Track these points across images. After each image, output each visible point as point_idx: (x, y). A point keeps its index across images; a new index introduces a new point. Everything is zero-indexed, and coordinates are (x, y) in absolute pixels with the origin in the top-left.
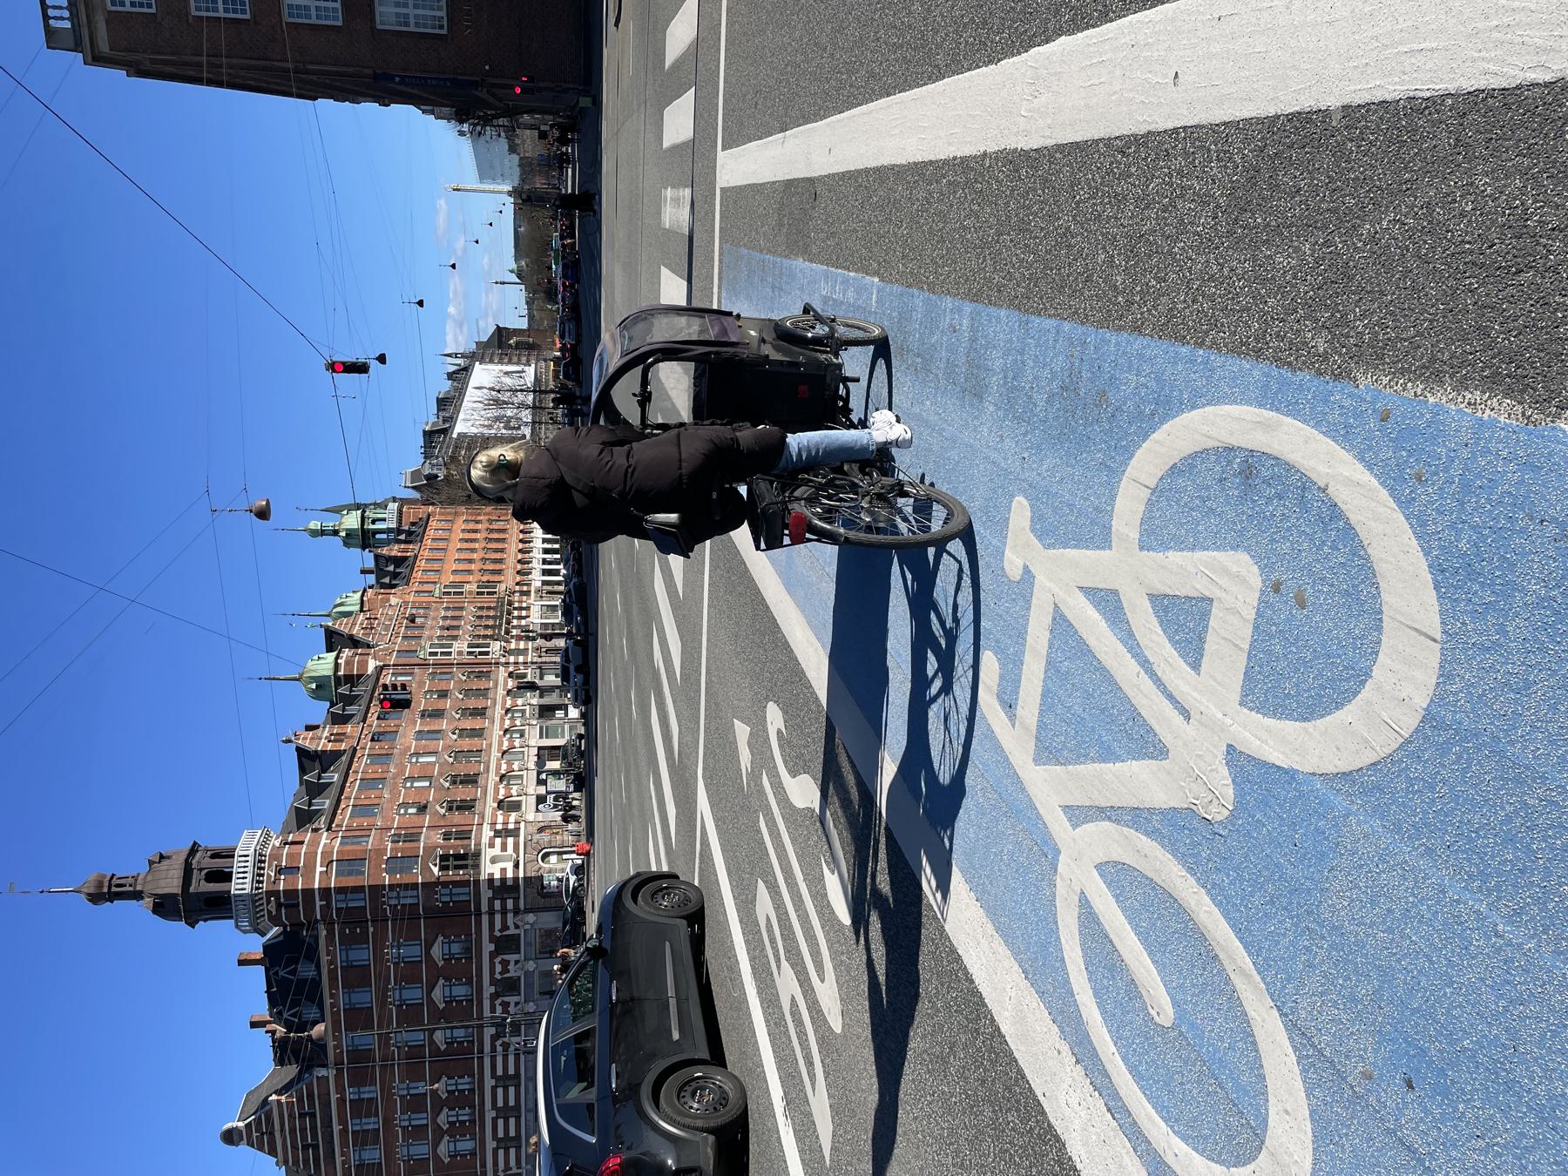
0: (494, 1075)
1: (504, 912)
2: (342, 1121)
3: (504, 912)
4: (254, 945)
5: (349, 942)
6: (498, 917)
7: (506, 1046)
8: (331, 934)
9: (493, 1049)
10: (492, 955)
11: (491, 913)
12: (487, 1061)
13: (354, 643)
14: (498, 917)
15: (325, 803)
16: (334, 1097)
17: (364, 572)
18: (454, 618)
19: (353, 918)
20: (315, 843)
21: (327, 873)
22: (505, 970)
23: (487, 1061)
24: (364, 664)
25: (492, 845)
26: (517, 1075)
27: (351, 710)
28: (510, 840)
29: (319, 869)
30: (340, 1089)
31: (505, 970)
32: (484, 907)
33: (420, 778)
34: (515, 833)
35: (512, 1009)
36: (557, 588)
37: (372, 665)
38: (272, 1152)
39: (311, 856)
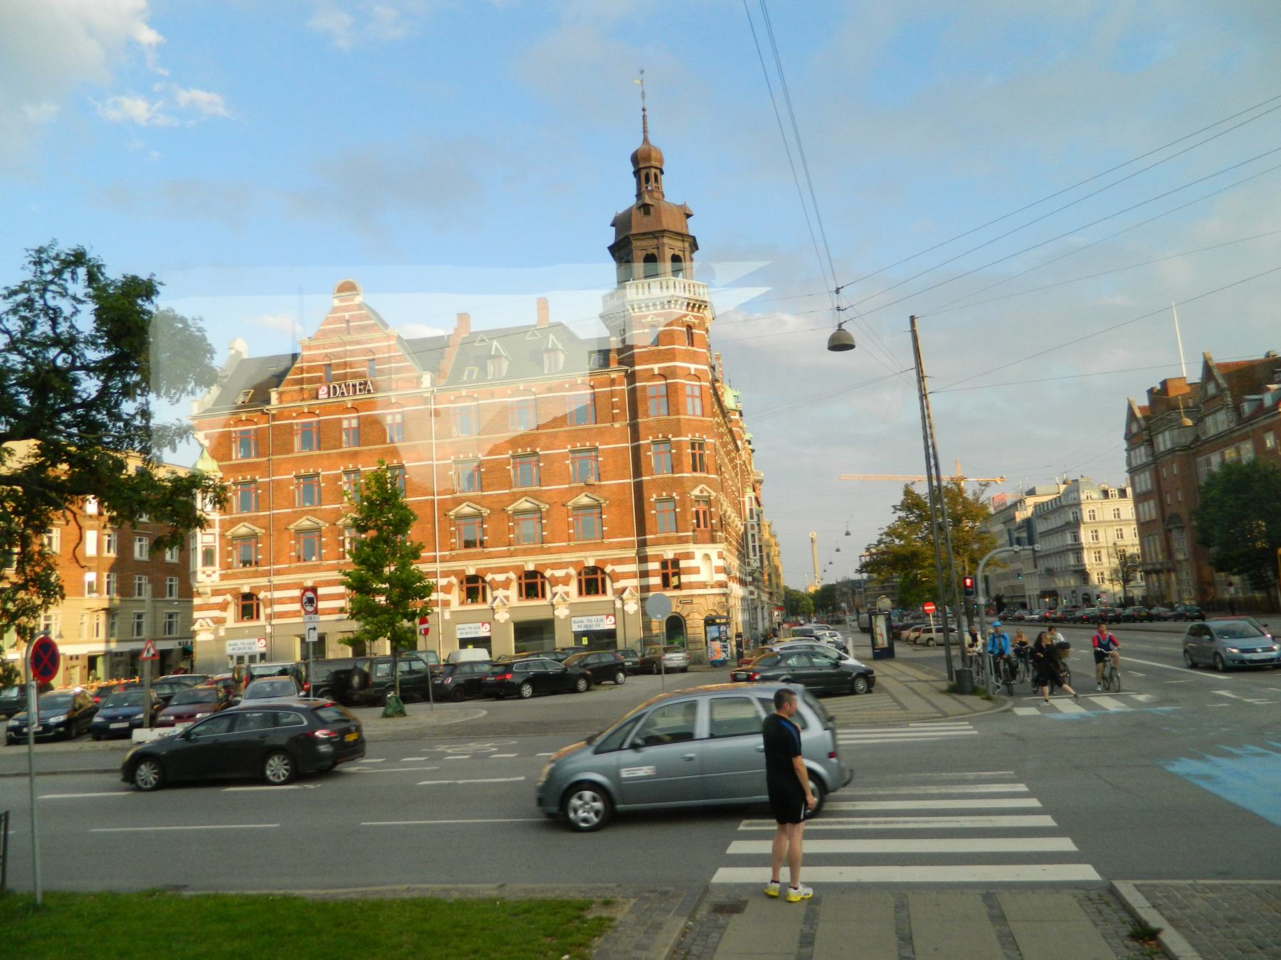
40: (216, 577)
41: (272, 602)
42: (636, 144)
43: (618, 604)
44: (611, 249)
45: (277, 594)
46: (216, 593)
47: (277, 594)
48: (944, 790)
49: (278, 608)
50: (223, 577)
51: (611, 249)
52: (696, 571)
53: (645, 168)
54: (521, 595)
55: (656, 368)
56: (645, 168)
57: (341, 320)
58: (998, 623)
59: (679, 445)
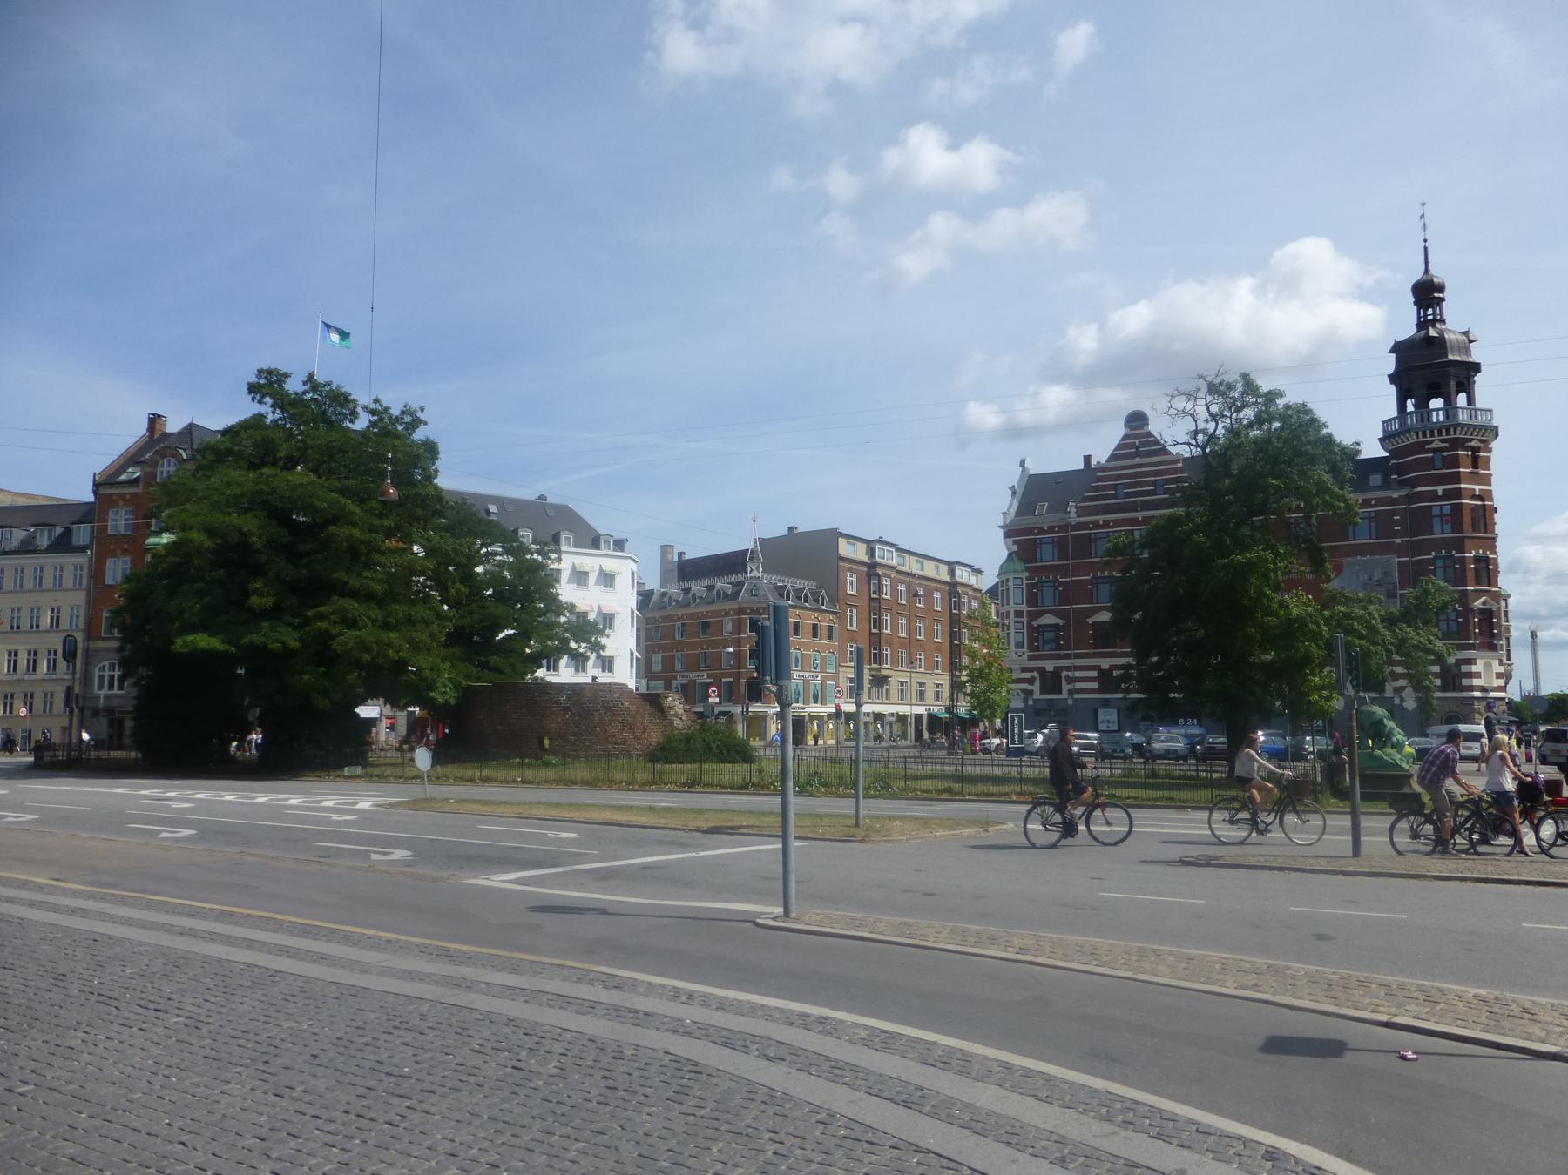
5: (1382, 524)
7: (1031, 681)
29: (1477, 488)
38: (1113, 457)
40: (1025, 657)
41: (1070, 680)
42: (1418, 275)
43: (1397, 701)
44: (1390, 377)
45: (1078, 674)
46: (1024, 670)
47: (1078, 674)
48: (237, 931)
49: (1079, 685)
50: (1031, 658)
51: (1390, 377)
52: (1478, 675)
53: (1427, 294)
54: (688, 570)
55: (1440, 489)
56: (1427, 294)
57: (1133, 446)
58: (1439, 645)
59: (1463, 561)
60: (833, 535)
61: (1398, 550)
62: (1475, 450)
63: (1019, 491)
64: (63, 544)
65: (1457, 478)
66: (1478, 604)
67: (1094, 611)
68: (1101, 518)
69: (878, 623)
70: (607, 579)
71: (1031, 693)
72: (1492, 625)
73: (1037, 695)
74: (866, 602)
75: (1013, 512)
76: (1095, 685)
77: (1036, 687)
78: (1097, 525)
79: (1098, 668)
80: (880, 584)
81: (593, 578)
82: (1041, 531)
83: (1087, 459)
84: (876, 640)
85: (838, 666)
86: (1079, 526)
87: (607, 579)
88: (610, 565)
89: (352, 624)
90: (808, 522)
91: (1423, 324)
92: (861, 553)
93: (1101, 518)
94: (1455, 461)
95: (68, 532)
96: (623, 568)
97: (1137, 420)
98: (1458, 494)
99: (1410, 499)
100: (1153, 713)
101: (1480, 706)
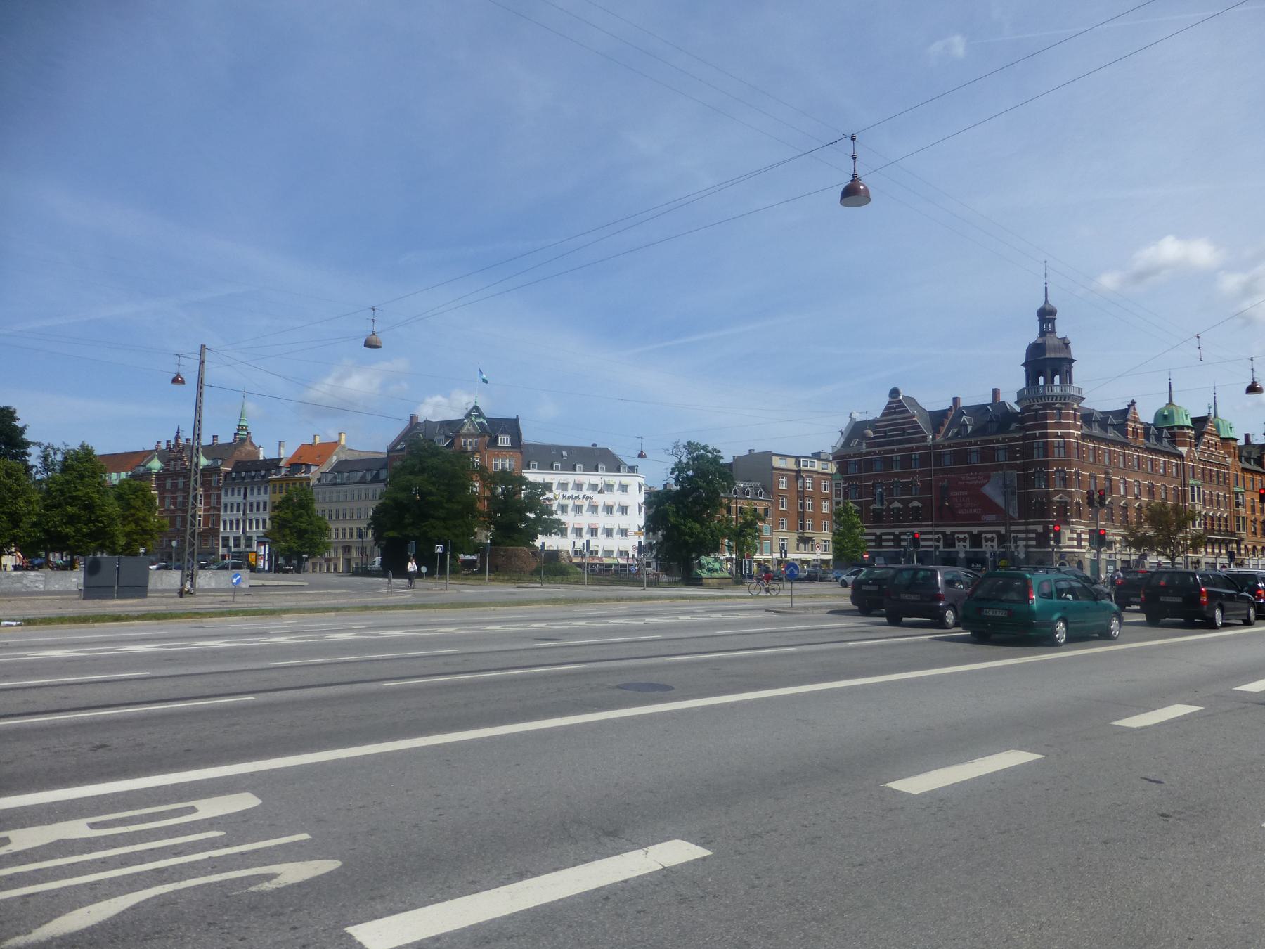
0: (901, 533)
1: (1027, 539)
2: (899, 451)
3: (1027, 539)
4: (1010, 399)
5: (1011, 451)
6: (1023, 536)
7: (938, 540)
8: (1017, 439)
9: (937, 533)
10: (970, 533)
11: (1027, 532)
12: (929, 529)
13: (1198, 437)
14: (1023, 536)
15: (1096, 431)
16: (914, 445)
17: (1247, 436)
18: (1211, 500)
19: (1027, 451)
20: (1075, 427)
21: (1056, 436)
22: (960, 540)
23: (929, 529)
24: (1183, 444)
25: (1072, 532)
26: (881, 547)
27: (1152, 438)
28: (1075, 543)
29: (1059, 431)
30: (918, 449)
31: (960, 540)
32: (1031, 527)
33: (1126, 488)
34: (1080, 546)
35: (989, 543)
36: (341, 536)
37: (1184, 450)
38: (884, 414)
39: (1068, 426)
42: (1040, 304)
53: (1046, 316)
56: (1046, 316)
60: (770, 455)
61: (1017, 468)
62: (1059, 409)
63: (846, 434)
64: (376, 479)
65: (1045, 426)
66: (1056, 498)
67: (912, 500)
68: (877, 449)
69: (803, 506)
70: (624, 488)
71: (937, 547)
72: (1066, 511)
73: (941, 549)
74: (794, 494)
75: (839, 446)
76: (922, 543)
77: (941, 544)
78: (875, 454)
79: (874, 534)
80: (804, 483)
81: (616, 487)
82: (850, 456)
83: (956, 400)
84: (802, 516)
85: (772, 531)
86: (868, 454)
87: (624, 488)
88: (625, 480)
89: (434, 528)
90: (759, 449)
91: (1043, 333)
92: (791, 464)
93: (877, 449)
94: (1045, 417)
95: (378, 474)
96: (633, 481)
97: (895, 392)
98: (1046, 435)
99: (1025, 438)
100: (576, 560)
101: (1056, 557)
